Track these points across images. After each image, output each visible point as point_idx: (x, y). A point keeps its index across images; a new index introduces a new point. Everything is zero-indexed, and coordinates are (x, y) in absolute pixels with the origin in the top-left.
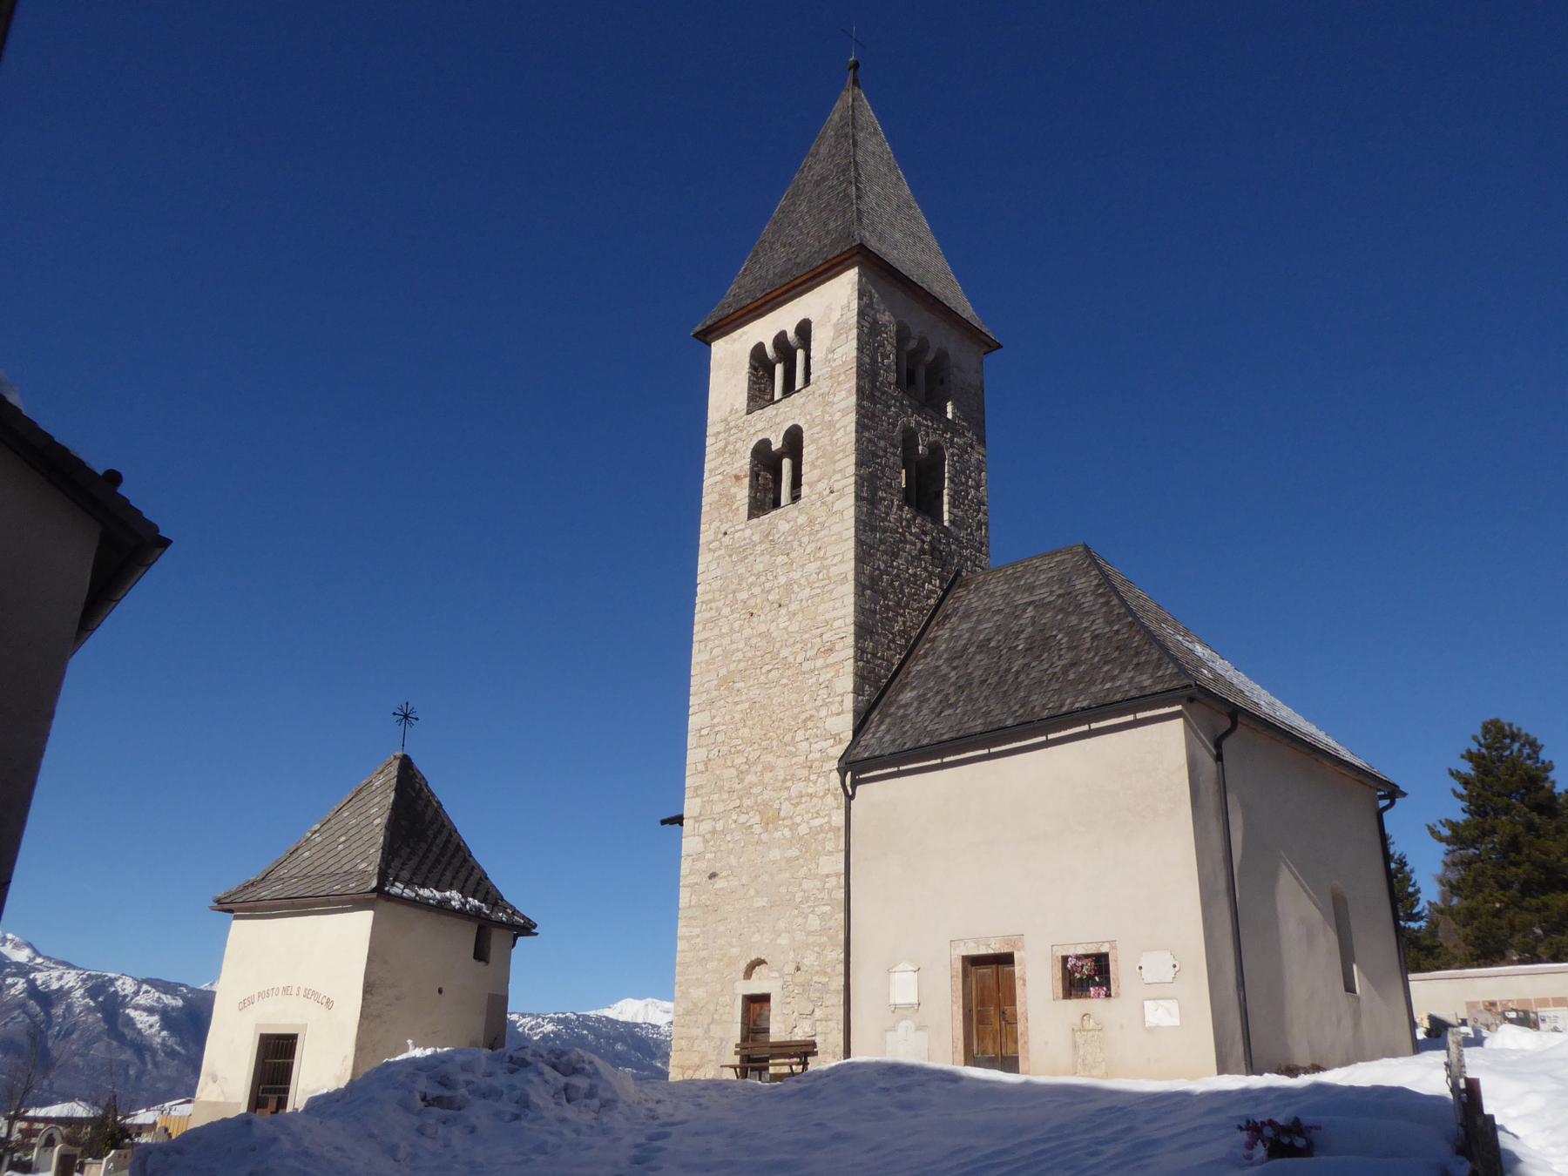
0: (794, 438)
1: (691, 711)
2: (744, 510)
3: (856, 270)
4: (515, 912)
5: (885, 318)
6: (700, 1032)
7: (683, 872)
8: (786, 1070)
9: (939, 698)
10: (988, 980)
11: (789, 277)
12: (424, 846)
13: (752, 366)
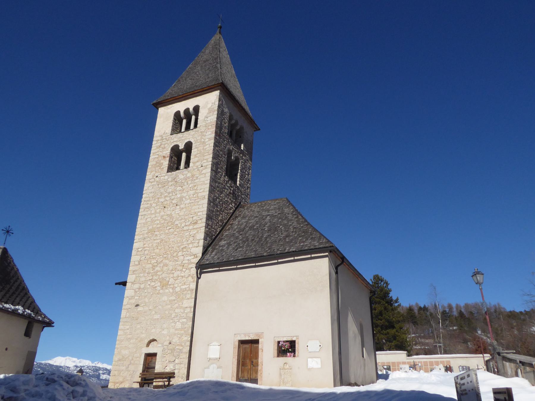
0: (189, 147)
2: (166, 169)
4: (45, 317)
5: (226, 110)
6: (124, 368)
7: (124, 304)
8: (161, 384)
9: (236, 244)
10: (248, 349)
11: (193, 90)
12: (8, 286)
13: (174, 119)
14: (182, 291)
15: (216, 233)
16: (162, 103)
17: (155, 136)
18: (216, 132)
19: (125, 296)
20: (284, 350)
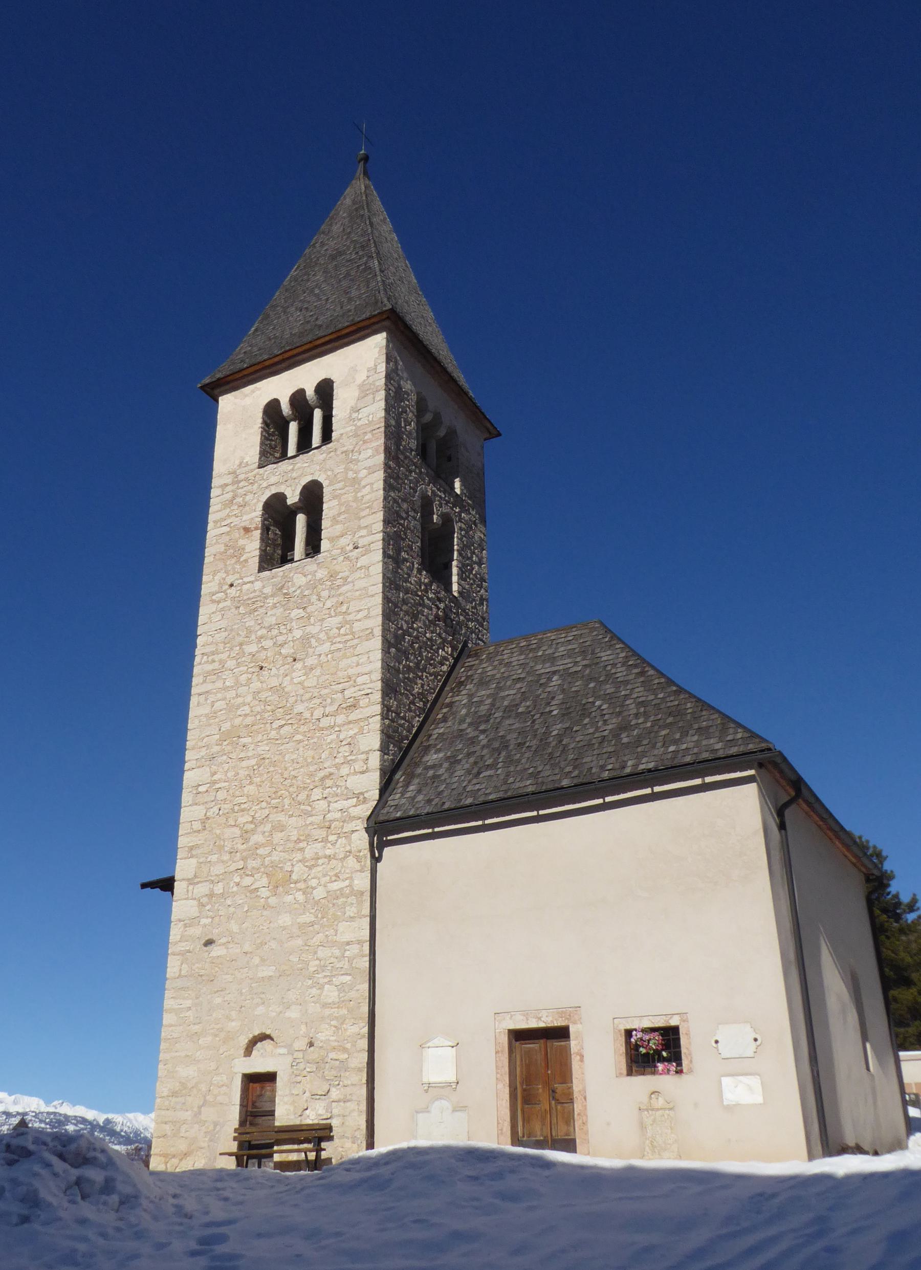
1: (187, 766)
2: (255, 562)
3: (384, 334)
5: (407, 386)
6: (188, 1115)
7: (172, 938)
8: (294, 1157)
9: (472, 760)
10: (539, 1057)
11: (310, 338)
13: (264, 422)
14: (332, 897)
15: (409, 731)
16: (228, 383)
17: (215, 473)
18: (387, 450)
19: (173, 918)
20: (647, 1054)
